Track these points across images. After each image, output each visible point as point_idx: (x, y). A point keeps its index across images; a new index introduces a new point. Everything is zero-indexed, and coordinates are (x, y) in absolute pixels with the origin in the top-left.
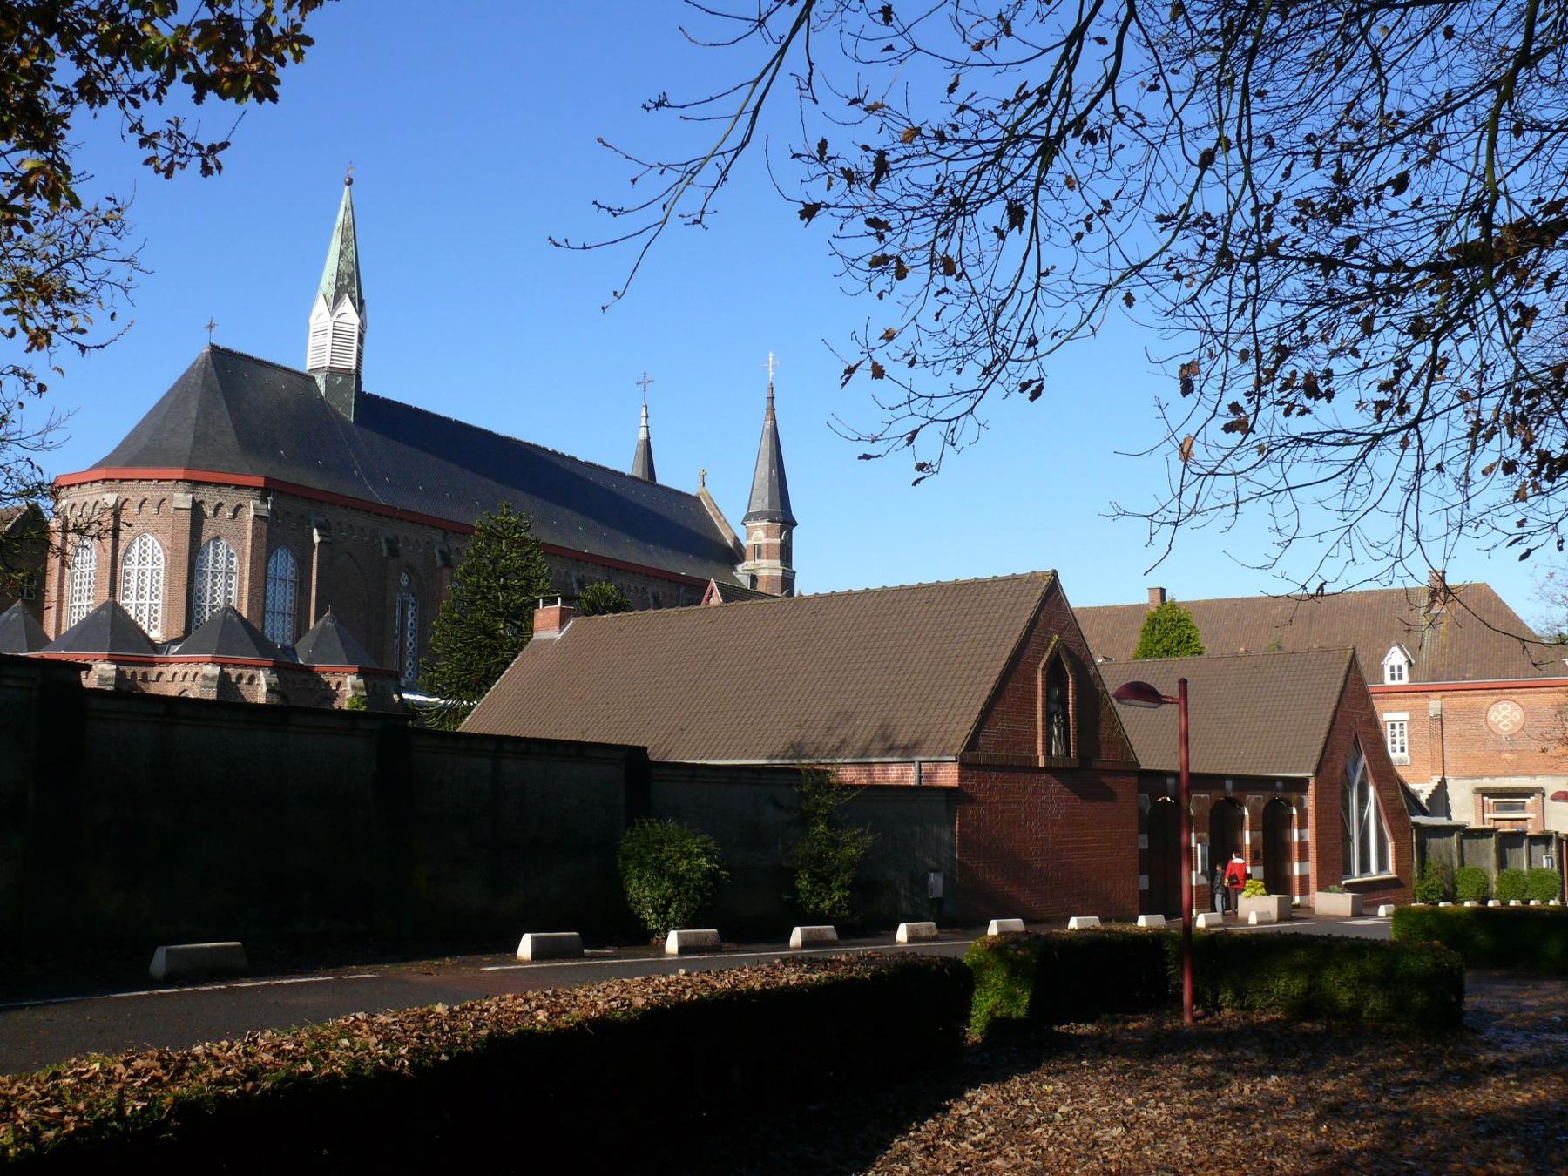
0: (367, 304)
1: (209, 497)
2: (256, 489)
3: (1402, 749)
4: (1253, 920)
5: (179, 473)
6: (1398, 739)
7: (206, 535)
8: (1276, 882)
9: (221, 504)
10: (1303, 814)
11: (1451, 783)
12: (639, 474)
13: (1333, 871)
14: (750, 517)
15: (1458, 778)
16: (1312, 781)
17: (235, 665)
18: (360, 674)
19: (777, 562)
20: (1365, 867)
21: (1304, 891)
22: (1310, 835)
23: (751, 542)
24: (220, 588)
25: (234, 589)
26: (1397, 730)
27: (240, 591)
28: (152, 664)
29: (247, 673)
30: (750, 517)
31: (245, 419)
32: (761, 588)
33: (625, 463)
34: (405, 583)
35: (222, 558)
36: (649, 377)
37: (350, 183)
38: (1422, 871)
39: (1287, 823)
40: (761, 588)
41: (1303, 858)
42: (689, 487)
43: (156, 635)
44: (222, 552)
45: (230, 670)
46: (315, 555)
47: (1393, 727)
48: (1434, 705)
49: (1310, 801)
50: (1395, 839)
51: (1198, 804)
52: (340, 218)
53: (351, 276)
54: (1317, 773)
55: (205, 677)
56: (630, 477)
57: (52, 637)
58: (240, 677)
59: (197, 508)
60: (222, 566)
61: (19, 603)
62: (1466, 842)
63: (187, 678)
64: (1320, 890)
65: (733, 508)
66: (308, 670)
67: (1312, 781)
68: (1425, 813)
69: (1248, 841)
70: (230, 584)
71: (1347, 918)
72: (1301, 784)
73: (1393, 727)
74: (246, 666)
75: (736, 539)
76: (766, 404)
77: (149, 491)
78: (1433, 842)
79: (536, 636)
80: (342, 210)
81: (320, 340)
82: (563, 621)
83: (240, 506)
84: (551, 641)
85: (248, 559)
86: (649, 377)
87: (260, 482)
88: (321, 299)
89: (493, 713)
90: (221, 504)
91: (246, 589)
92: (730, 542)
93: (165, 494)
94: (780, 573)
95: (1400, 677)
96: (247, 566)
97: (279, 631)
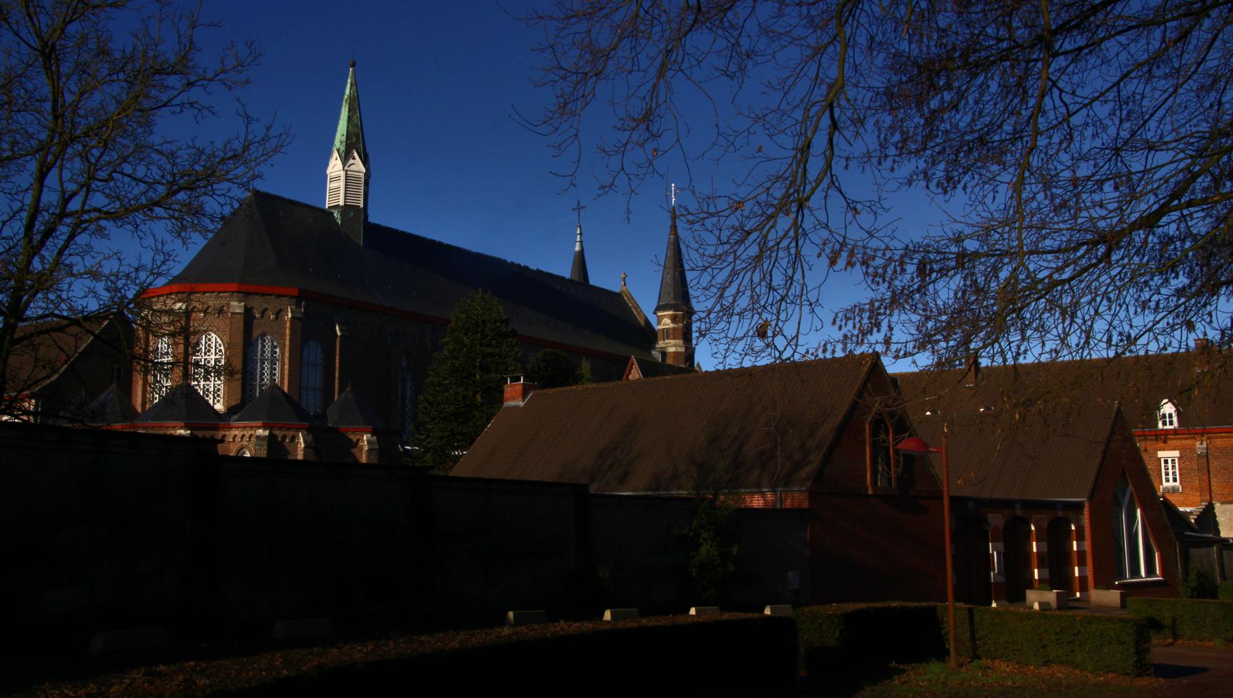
0: (370, 157)
1: (257, 303)
2: (292, 297)
3: (1175, 480)
4: (1036, 606)
5: (235, 287)
6: (1170, 471)
7: (256, 332)
8: (1058, 578)
9: (266, 310)
10: (1080, 529)
11: (1218, 508)
12: (576, 278)
13: (1107, 573)
14: (659, 308)
15: (1223, 503)
16: (1087, 505)
17: (280, 428)
18: (373, 433)
19: (681, 342)
20: (1135, 571)
21: (1083, 589)
22: (1087, 546)
23: (660, 327)
24: (267, 372)
25: (277, 372)
26: (1170, 465)
27: (282, 373)
28: (217, 429)
29: (290, 433)
30: (659, 308)
31: (287, 248)
32: (669, 361)
33: (563, 269)
34: (404, 364)
35: (268, 349)
36: (582, 204)
37: (353, 65)
38: (1186, 572)
39: (1068, 536)
40: (669, 361)
41: (1082, 564)
42: (615, 287)
43: (219, 407)
44: (268, 345)
45: (277, 432)
46: (863, 605)
47: (1166, 462)
48: (1200, 446)
49: (1086, 520)
50: (1160, 550)
51: (996, 520)
52: (347, 92)
53: (357, 136)
54: (1090, 499)
55: (258, 437)
56: (570, 280)
57: (139, 410)
58: (284, 437)
59: (248, 312)
60: (268, 354)
61: (114, 386)
62: (1225, 553)
63: (245, 440)
64: (1096, 587)
65: (646, 297)
66: (337, 431)
67: (1087, 505)
68: (1193, 530)
69: (1035, 550)
70: (275, 370)
71: (1115, 608)
72: (1078, 507)
73: (1166, 462)
74: (289, 429)
75: (647, 321)
76: (669, 222)
77: (212, 301)
78: (1194, 552)
79: (506, 404)
80: (348, 86)
81: (334, 185)
82: (524, 395)
83: (280, 310)
84: (517, 407)
85: (287, 349)
86: (582, 204)
87: (296, 293)
88: (336, 154)
89: (467, 462)
90: (266, 310)
91: (286, 372)
92: (642, 323)
93: (224, 302)
94: (683, 350)
95: (1171, 423)
96: (287, 354)
97: (312, 403)
